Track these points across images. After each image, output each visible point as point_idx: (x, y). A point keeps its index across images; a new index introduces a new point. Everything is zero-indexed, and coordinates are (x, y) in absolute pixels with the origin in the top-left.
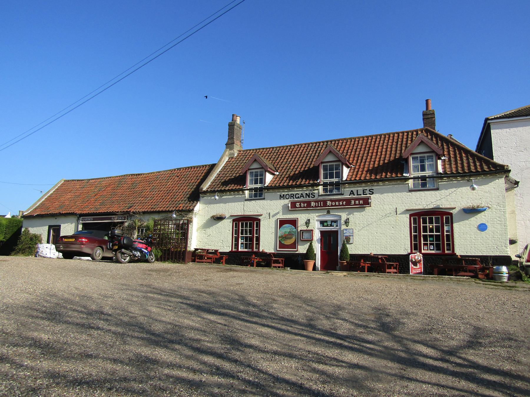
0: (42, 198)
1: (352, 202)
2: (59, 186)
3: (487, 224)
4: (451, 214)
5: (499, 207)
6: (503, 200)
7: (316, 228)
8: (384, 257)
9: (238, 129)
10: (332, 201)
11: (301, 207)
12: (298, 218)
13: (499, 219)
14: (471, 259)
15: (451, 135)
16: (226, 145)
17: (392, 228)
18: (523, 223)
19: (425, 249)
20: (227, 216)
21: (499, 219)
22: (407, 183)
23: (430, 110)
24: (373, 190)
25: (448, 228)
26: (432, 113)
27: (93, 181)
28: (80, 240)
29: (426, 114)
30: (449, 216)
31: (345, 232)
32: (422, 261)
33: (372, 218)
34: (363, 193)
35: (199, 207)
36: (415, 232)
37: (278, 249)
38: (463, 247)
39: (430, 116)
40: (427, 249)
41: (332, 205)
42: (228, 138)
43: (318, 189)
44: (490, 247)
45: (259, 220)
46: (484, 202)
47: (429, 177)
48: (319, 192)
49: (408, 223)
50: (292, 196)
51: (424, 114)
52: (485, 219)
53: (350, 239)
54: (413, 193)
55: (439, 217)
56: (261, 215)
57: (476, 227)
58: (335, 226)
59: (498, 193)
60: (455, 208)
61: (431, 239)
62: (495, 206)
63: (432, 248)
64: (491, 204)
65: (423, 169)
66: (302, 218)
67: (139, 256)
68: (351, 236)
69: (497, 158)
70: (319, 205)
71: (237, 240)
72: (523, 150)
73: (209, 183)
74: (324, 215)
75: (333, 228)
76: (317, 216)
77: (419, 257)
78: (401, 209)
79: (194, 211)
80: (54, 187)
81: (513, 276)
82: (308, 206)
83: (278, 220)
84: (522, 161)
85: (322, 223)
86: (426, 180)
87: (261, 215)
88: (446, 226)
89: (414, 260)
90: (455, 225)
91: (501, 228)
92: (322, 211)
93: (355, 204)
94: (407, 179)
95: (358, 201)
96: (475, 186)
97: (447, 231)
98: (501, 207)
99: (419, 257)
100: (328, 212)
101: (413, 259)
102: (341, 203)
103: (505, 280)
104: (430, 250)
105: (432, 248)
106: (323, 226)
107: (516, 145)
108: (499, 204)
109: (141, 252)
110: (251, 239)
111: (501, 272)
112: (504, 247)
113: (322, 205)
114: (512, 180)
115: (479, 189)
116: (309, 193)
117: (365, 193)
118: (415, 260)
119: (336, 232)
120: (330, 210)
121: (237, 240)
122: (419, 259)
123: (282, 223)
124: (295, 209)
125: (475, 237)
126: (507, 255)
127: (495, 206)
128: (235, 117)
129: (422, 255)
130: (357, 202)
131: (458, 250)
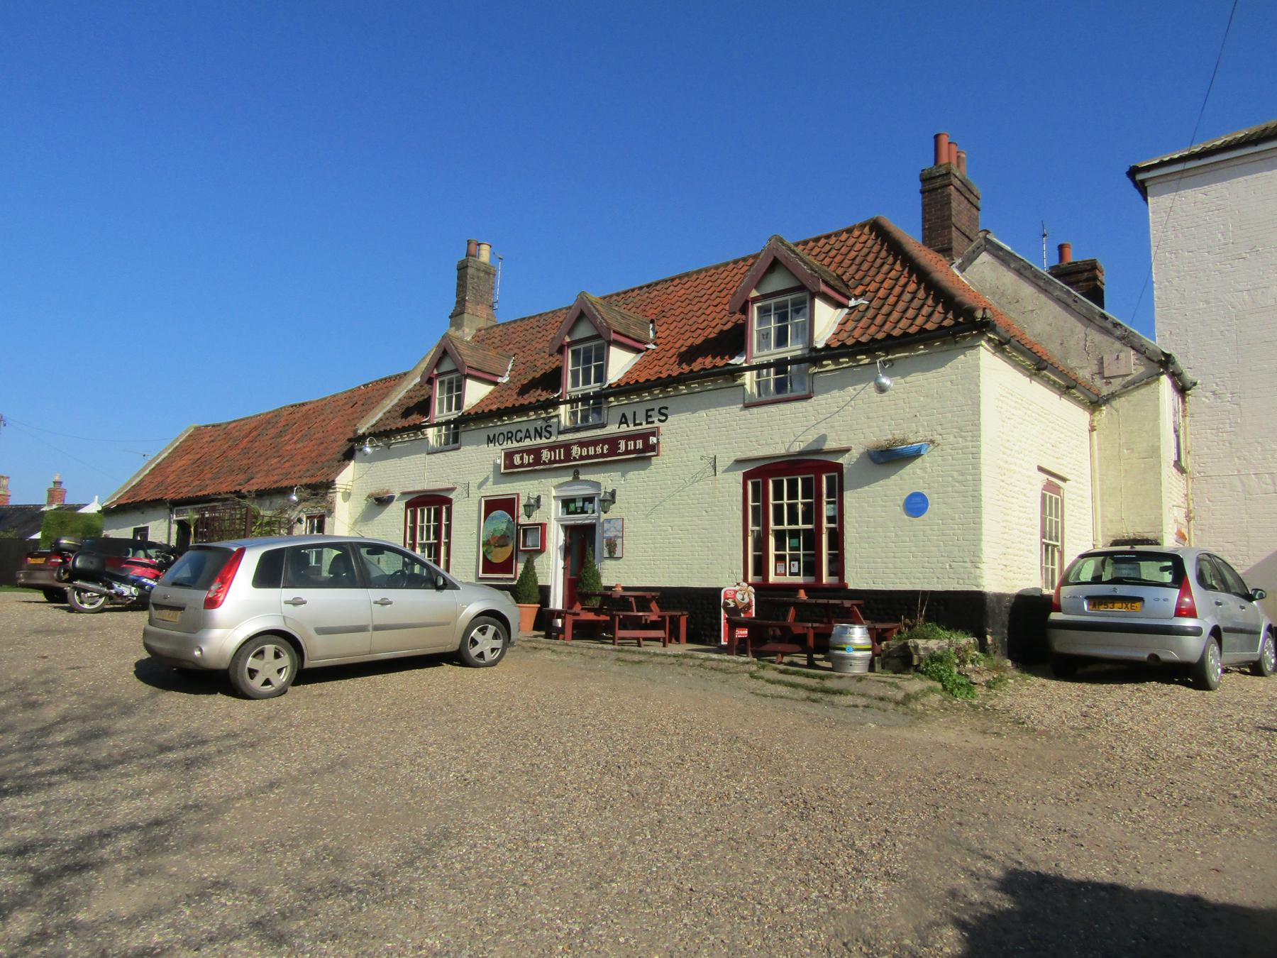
0: (145, 468)
1: (621, 446)
2: (181, 440)
3: (926, 492)
4: (839, 468)
5: (960, 439)
6: (972, 417)
7: (553, 517)
8: (636, 597)
9: (482, 274)
10: (582, 444)
11: (522, 465)
12: (518, 494)
13: (960, 478)
14: (825, 601)
15: (988, 232)
16: (450, 317)
17: (704, 513)
18: (1238, 484)
19: (778, 572)
20: (397, 495)
21: (960, 478)
22: (739, 381)
23: (941, 166)
24: (666, 408)
25: (834, 509)
26: (944, 172)
27: (233, 425)
28: (54, 560)
29: (928, 176)
30: (836, 474)
31: (606, 526)
32: (754, 607)
33: (664, 486)
34: (647, 420)
35: (348, 477)
36: (756, 523)
37: (481, 575)
38: (866, 565)
39: (939, 182)
40: (783, 572)
41: (582, 458)
42: (456, 299)
43: (557, 416)
44: (933, 566)
45: (448, 502)
46: (923, 426)
47: (795, 361)
48: (559, 422)
49: (740, 498)
50: (510, 437)
51: (926, 179)
52: (923, 478)
53: (616, 545)
54: (755, 410)
55: (835, 476)
56: (452, 490)
57: (901, 503)
58: (590, 511)
59: (960, 398)
60: (847, 450)
61: (795, 542)
62: (952, 439)
63: (795, 570)
64: (940, 431)
65: (782, 340)
66: (524, 489)
67: (133, 596)
68: (619, 537)
69: (1166, 287)
70: (557, 458)
71: (761, 544)
72: (1244, 255)
73: (380, 415)
74: (567, 483)
75: (587, 518)
76: (557, 487)
77: (746, 596)
78: (725, 460)
79: (337, 486)
80: (172, 444)
81: (893, 658)
82: (536, 464)
83: (516, 497)
84: (1240, 288)
85: (567, 503)
86: (785, 372)
87: (452, 490)
88: (828, 503)
89: (732, 605)
90: (848, 496)
91: (964, 507)
92: (562, 472)
93: (627, 452)
94: (740, 370)
95: (632, 442)
96: (885, 381)
97: (831, 519)
98: (966, 441)
99: (746, 596)
100: (576, 478)
101: (729, 601)
102: (599, 450)
103: (858, 669)
104: (791, 574)
105: (795, 570)
106: (568, 513)
107: (1223, 242)
108: (961, 430)
109: (141, 586)
110: (812, 540)
111: (841, 644)
112: (969, 565)
113: (562, 458)
114: (1153, 351)
115: (913, 389)
116: (541, 428)
117: (650, 420)
118: (736, 606)
119: (591, 528)
120: (580, 470)
121: (761, 544)
122: (747, 600)
123: (492, 506)
124: (511, 470)
125: (897, 535)
126: (975, 589)
127: (952, 439)
128: (473, 247)
129: (753, 590)
130: (631, 445)
131: (854, 574)
